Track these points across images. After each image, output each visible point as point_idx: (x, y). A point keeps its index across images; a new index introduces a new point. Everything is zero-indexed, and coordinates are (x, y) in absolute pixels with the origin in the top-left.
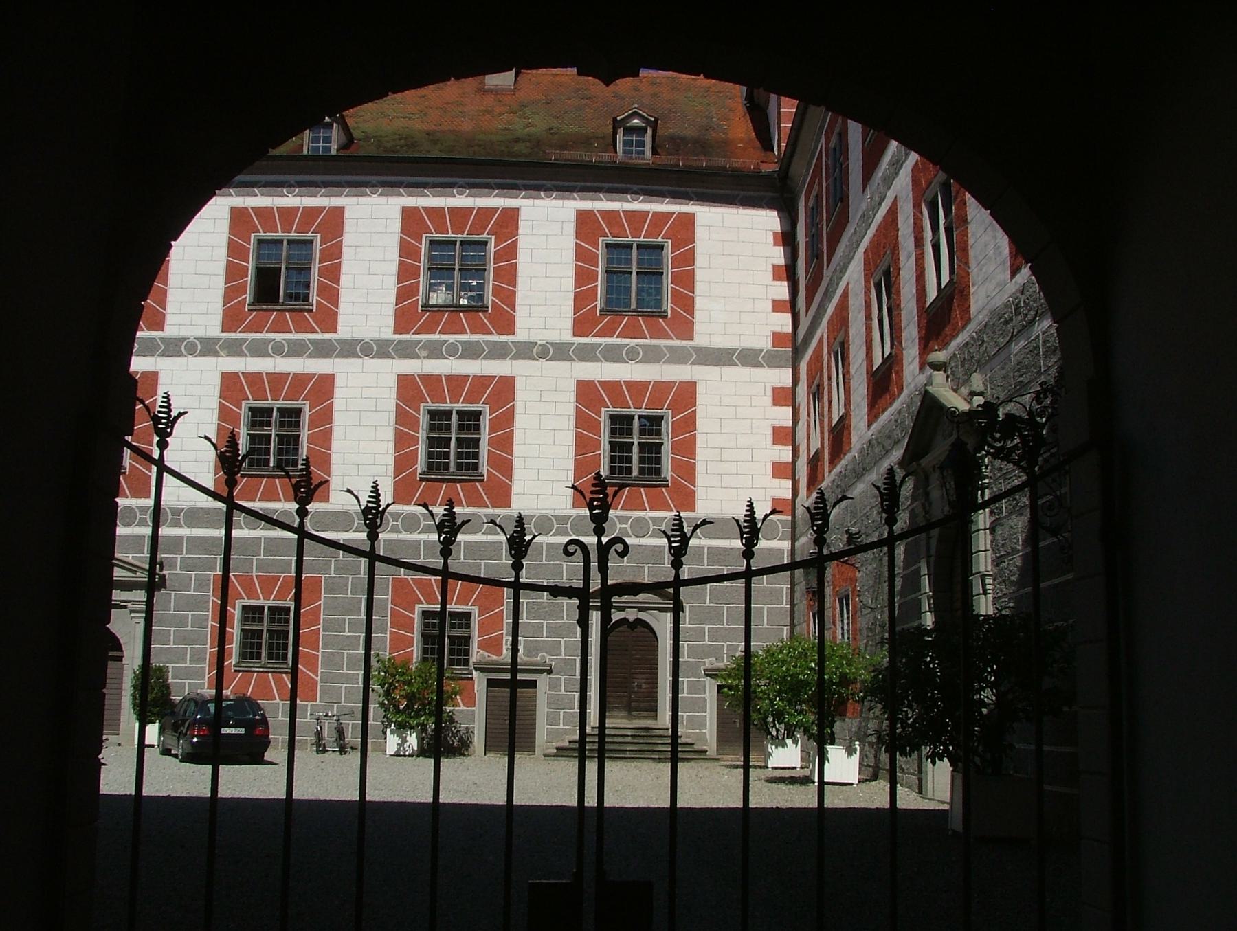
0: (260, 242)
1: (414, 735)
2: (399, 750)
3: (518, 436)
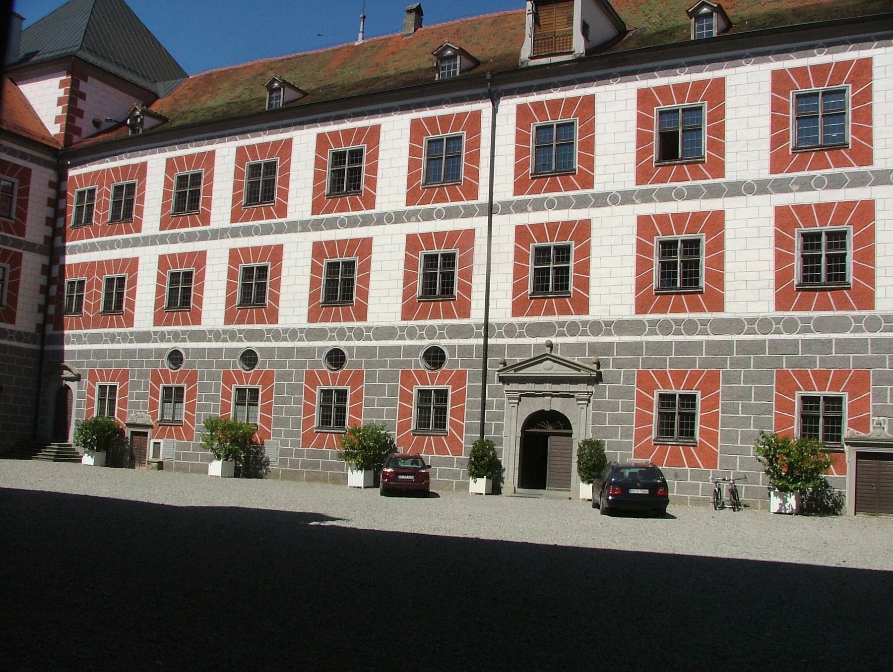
0: (661, 113)
1: (793, 497)
2: (781, 508)
3: (879, 250)
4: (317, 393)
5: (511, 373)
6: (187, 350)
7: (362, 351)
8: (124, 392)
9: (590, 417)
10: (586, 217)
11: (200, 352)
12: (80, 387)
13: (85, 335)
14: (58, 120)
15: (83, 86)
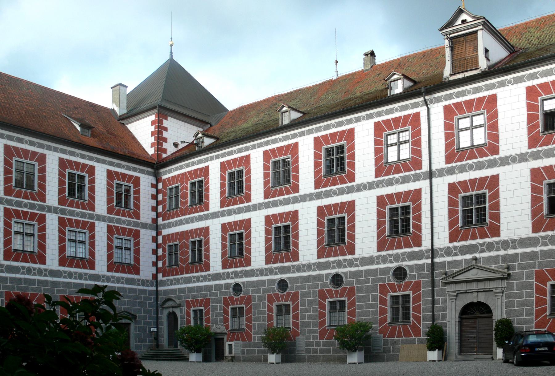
4: (327, 304)
5: (450, 280)
6: (244, 283)
7: (353, 274)
8: (208, 313)
9: (504, 304)
10: (495, 174)
11: (252, 284)
12: (181, 312)
13: (181, 278)
14: (152, 145)
15: (165, 123)
